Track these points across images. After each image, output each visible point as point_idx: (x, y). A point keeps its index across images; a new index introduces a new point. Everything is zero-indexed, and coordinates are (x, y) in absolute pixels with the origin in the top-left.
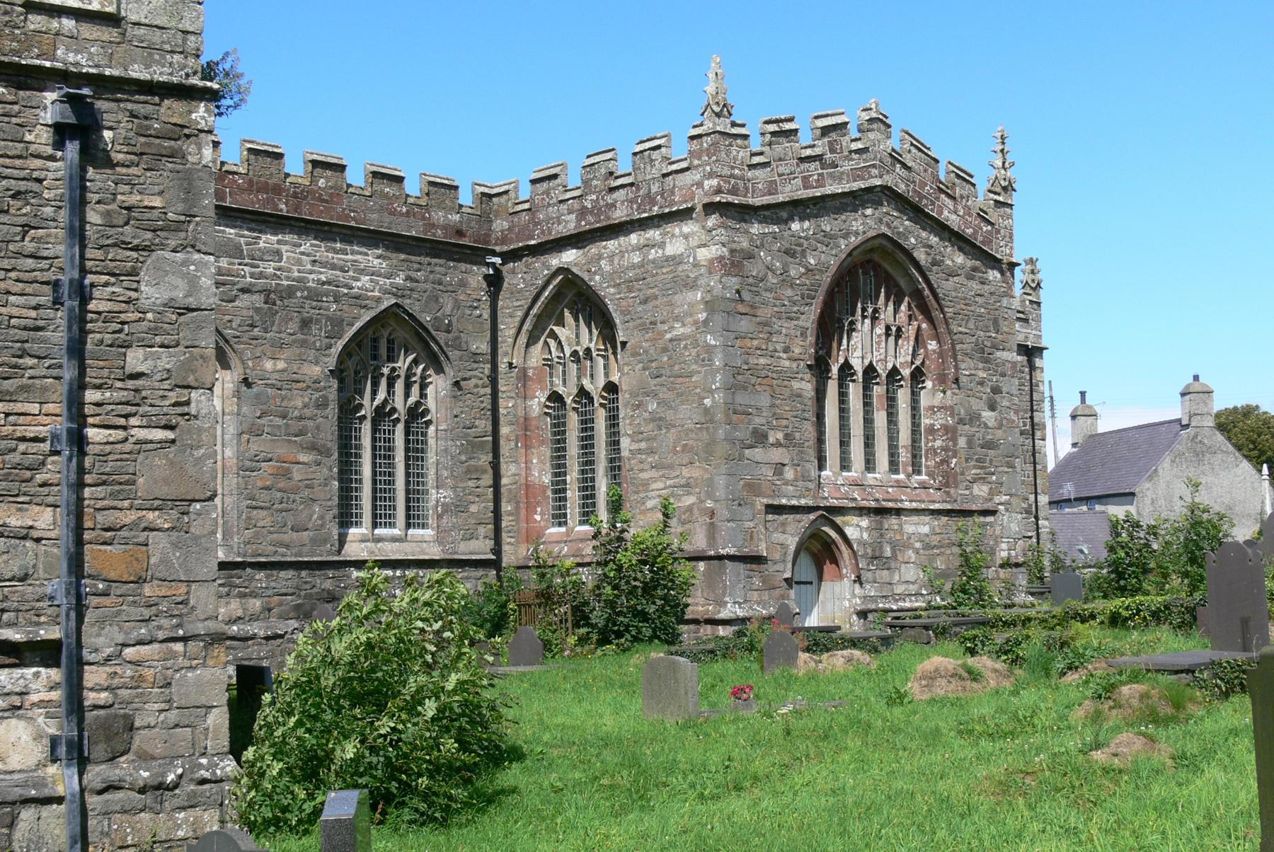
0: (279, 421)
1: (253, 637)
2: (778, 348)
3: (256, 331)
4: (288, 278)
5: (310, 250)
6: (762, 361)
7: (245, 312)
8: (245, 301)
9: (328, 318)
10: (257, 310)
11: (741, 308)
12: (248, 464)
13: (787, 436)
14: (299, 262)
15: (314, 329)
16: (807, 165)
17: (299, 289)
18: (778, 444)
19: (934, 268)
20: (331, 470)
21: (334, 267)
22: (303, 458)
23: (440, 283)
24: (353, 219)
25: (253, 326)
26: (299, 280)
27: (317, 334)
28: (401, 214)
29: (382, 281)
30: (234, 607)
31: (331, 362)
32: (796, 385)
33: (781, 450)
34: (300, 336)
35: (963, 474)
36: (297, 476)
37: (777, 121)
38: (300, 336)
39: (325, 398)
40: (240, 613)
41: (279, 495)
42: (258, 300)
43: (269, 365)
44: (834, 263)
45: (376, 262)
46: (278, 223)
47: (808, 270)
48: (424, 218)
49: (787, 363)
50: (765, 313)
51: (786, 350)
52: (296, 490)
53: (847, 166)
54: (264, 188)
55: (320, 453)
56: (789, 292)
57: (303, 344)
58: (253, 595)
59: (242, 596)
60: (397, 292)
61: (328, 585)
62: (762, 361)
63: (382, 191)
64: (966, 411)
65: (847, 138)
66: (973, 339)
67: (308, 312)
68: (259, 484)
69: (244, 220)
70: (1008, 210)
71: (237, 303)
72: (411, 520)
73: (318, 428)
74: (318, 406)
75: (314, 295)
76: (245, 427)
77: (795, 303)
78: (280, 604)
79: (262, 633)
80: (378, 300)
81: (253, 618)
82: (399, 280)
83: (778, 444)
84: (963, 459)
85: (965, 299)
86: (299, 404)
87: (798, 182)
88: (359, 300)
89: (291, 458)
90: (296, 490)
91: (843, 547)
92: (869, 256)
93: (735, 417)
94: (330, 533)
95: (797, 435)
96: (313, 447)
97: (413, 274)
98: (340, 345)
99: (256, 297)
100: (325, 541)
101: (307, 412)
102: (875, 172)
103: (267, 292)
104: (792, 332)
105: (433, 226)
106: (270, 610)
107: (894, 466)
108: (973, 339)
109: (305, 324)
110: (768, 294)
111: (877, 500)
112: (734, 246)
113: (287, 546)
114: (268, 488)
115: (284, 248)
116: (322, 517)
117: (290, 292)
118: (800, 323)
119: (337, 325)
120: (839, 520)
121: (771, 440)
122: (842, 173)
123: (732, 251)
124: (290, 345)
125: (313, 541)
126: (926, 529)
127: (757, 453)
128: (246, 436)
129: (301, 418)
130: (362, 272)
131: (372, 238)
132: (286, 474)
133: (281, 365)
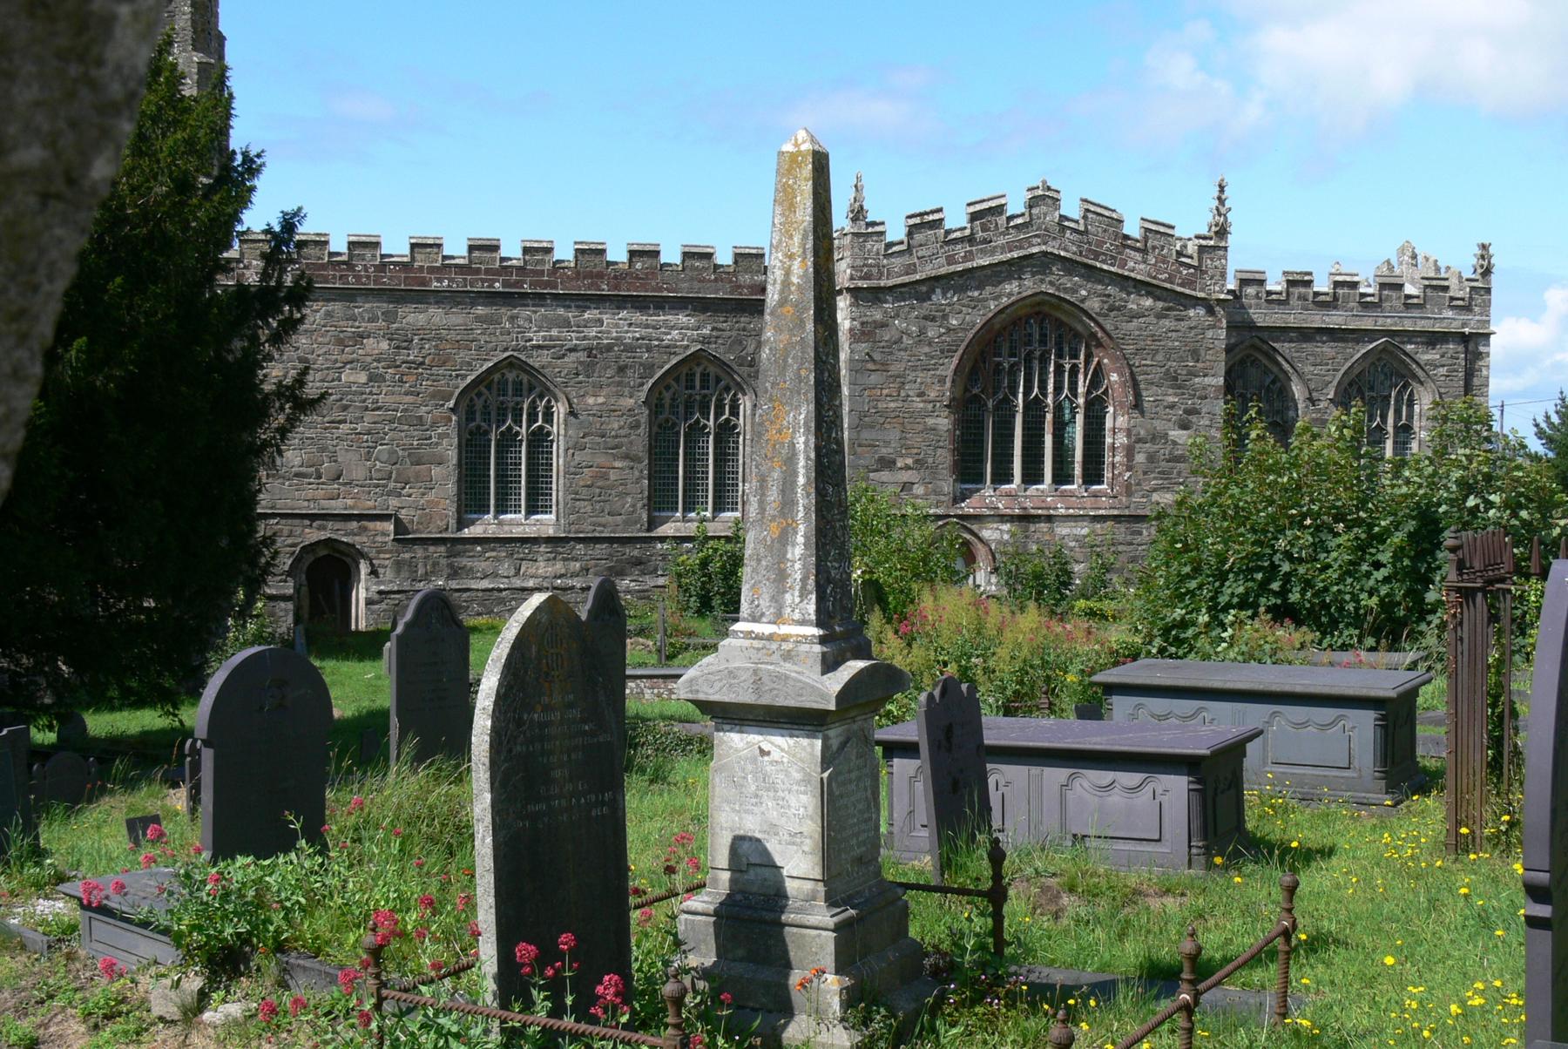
0: (598, 439)
1: (573, 588)
2: (911, 393)
3: (581, 378)
4: (607, 338)
5: (628, 316)
6: (892, 405)
7: (571, 365)
8: (572, 357)
9: (641, 364)
10: (581, 363)
11: (870, 366)
12: (572, 470)
13: (917, 462)
14: (617, 325)
15: (629, 372)
16: (951, 247)
17: (617, 345)
18: (907, 468)
19: (1112, 314)
20: (641, 471)
21: (647, 326)
22: (618, 464)
23: (744, 329)
24: (666, 289)
25: (577, 374)
26: (617, 339)
27: (632, 377)
28: (710, 281)
29: (689, 333)
30: (559, 567)
31: (643, 396)
32: (930, 421)
33: (910, 472)
34: (617, 379)
35: (1138, 484)
36: (612, 477)
37: (921, 215)
38: (617, 379)
39: (638, 422)
40: (563, 571)
41: (598, 491)
42: (582, 356)
43: (591, 401)
44: (979, 322)
45: (685, 319)
46: (600, 300)
47: (949, 330)
48: (731, 281)
49: (921, 405)
50: (896, 368)
51: (921, 395)
52: (612, 487)
53: (1002, 241)
54: (590, 275)
55: (633, 460)
56: (927, 349)
57: (619, 384)
58: (575, 559)
59: (564, 560)
60: (705, 340)
61: (636, 553)
62: (892, 405)
63: (692, 265)
64: (1147, 431)
65: (1004, 217)
66: (1163, 370)
67: (625, 359)
68: (582, 483)
69: (572, 300)
70: (1221, 253)
71: (566, 359)
72: (1032, 475)
73: (631, 443)
74: (631, 428)
75: (630, 349)
76: (570, 444)
77: (932, 358)
78: (596, 566)
79: (579, 586)
80: (687, 347)
81: (574, 575)
82: (706, 331)
83: (907, 468)
84: (1140, 472)
85: (1153, 336)
86: (616, 426)
87: (943, 260)
88: (669, 349)
89: (608, 464)
90: (612, 487)
91: (980, 546)
92: (1037, 309)
93: (859, 450)
94: (640, 517)
95: (930, 460)
96: (626, 457)
97: (720, 325)
98: (651, 381)
99: (581, 353)
100: (636, 523)
101: (622, 432)
102: (1035, 241)
103: (589, 351)
104: (929, 380)
105: (740, 286)
106: (588, 570)
107: (1062, 476)
108: (1163, 370)
109: (622, 370)
110: (902, 353)
111: (1025, 509)
112: (865, 319)
113: (604, 526)
114: (588, 486)
115: (604, 317)
116: (634, 506)
117: (609, 348)
118: (938, 373)
119: (649, 368)
120: (975, 527)
121: (899, 465)
122: (996, 247)
123: (862, 324)
124: (608, 385)
125: (626, 523)
126: (1085, 531)
127: (885, 475)
128: (571, 451)
129: (616, 437)
130: (672, 328)
131: (680, 304)
132: (605, 477)
133: (601, 400)
